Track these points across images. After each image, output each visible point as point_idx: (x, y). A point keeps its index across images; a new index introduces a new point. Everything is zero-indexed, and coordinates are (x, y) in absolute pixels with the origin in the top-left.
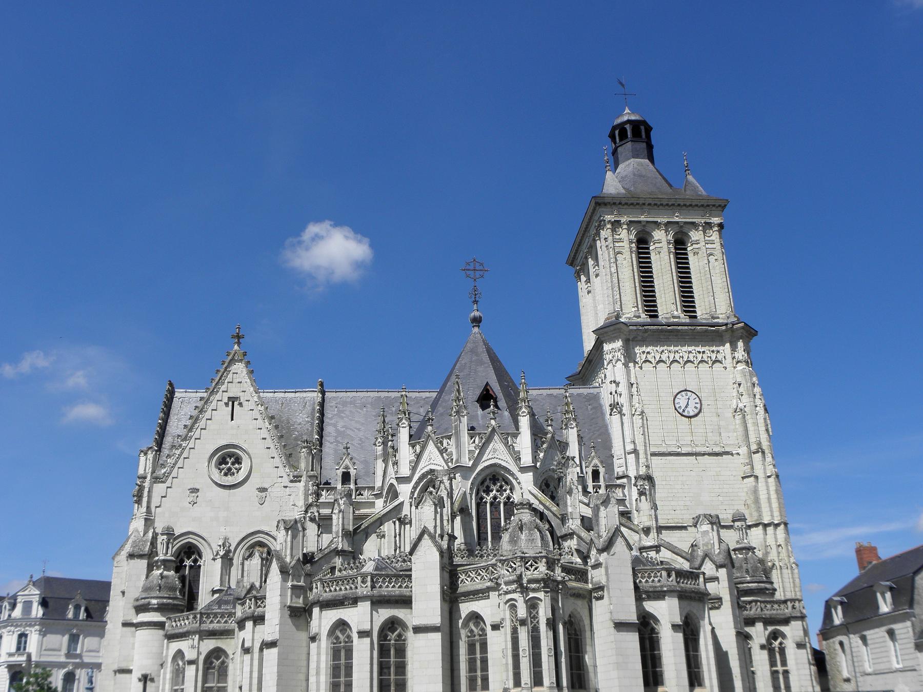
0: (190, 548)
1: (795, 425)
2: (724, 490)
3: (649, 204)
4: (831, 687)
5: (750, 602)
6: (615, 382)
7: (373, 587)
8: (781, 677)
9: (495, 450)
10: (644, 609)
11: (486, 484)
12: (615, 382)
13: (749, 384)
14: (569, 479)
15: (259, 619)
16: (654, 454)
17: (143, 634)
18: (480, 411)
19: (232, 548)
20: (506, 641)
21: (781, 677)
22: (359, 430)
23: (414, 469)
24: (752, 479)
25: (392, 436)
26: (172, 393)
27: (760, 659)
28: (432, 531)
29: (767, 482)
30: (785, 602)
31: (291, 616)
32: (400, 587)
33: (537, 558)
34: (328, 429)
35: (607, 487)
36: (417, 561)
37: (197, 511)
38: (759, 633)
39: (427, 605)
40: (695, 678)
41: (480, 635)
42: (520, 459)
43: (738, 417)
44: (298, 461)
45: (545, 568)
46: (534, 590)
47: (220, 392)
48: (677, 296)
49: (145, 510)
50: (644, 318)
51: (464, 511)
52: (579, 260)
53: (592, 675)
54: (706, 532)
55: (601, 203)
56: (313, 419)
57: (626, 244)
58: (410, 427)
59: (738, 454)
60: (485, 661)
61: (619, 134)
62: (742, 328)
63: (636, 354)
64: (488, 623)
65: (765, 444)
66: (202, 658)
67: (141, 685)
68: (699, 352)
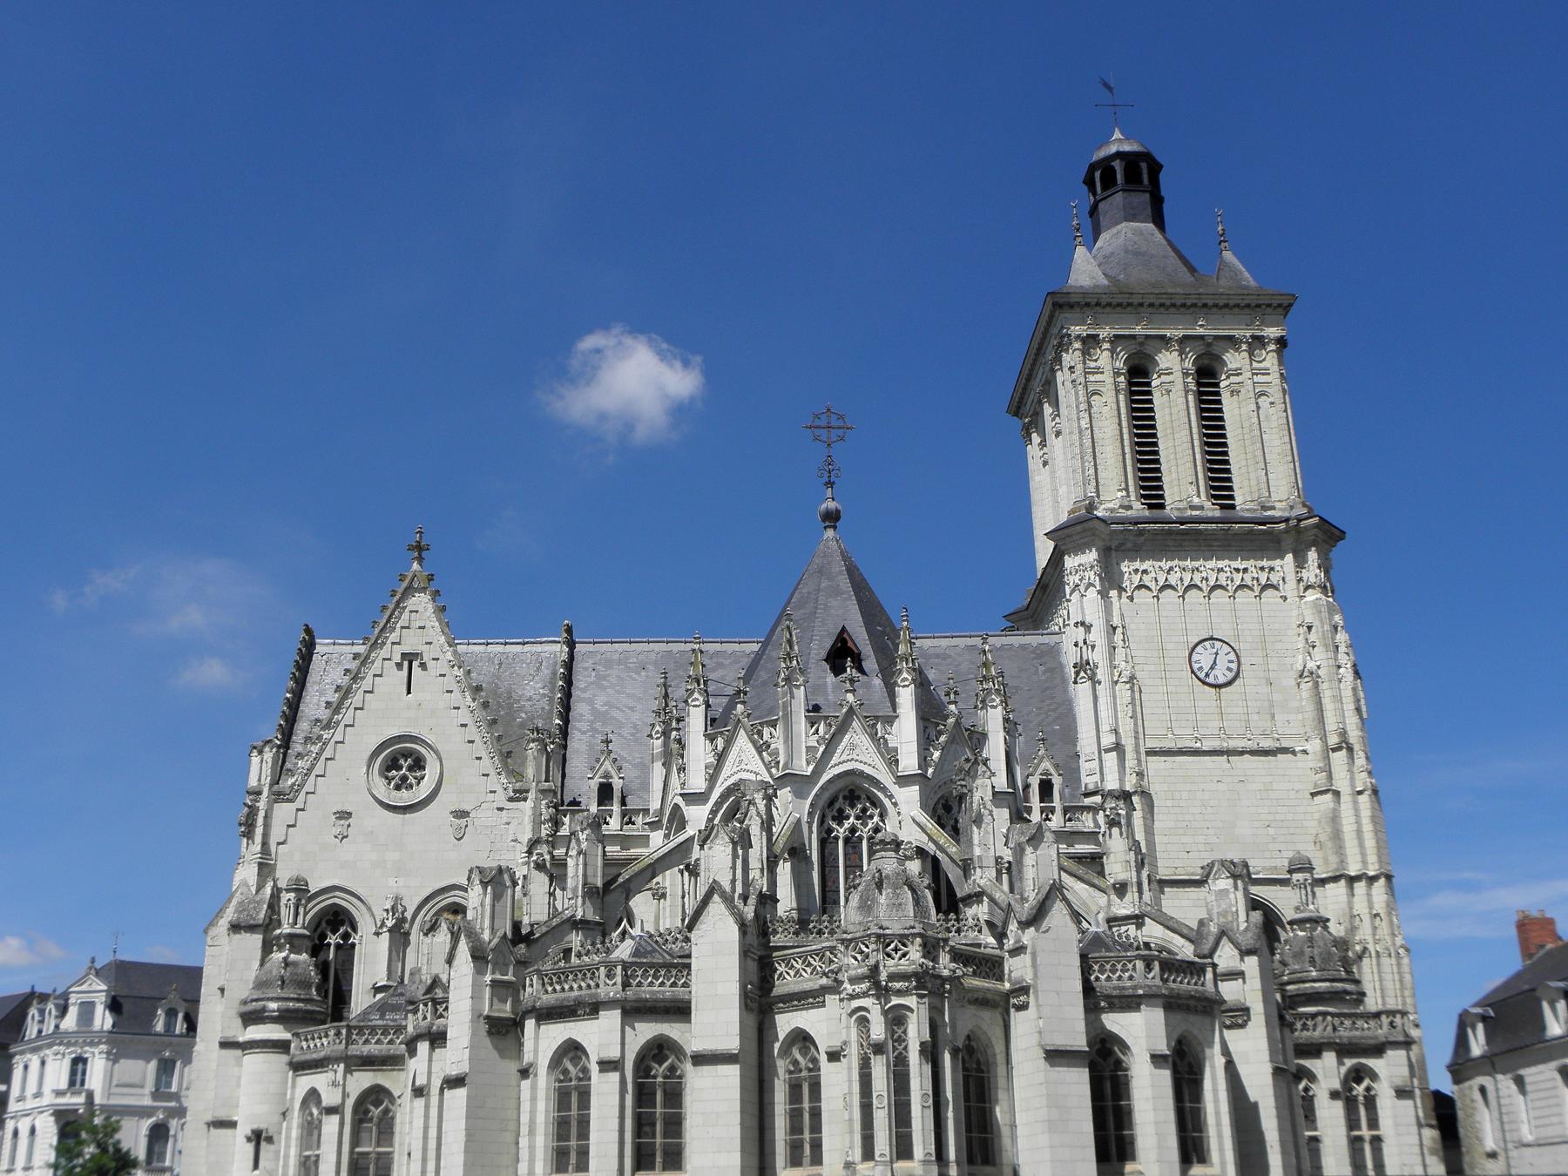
1: (1410, 704)
2: (1278, 817)
3: (1151, 305)
4: (1466, 1167)
5: (1314, 1016)
6: (1083, 624)
7: (626, 985)
9: (853, 747)
10: (1103, 1027)
11: (837, 806)
12: (1083, 624)
13: (1327, 627)
14: (976, 798)
15: (438, 1039)
16: (1151, 753)
17: (255, 1062)
18: (830, 678)
19: (408, 915)
20: (850, 1081)
22: (632, 709)
23: (712, 780)
24: (1329, 796)
25: (678, 720)
26: (308, 648)
27: (1330, 1119)
28: (728, 888)
29: (1355, 802)
30: (1377, 1015)
31: (490, 1033)
32: (674, 985)
33: (906, 936)
34: (579, 708)
35: (1066, 810)
37: (347, 850)
38: (1327, 1071)
39: (716, 1018)
40: (1191, 1147)
41: (810, 1070)
42: (897, 761)
43: (1306, 686)
44: (523, 764)
45: (919, 955)
46: (899, 993)
47: (389, 644)
48: (1199, 468)
49: (258, 848)
50: (1138, 509)
51: (796, 852)
52: (1028, 407)
53: (1006, 1141)
54: (1224, 892)
55: (1063, 303)
56: (552, 691)
57: (1107, 377)
58: (708, 706)
59: (1305, 752)
60: (816, 1114)
61: (1102, 177)
62: (1316, 526)
63: (1122, 574)
64: (822, 1049)
65: (1354, 735)
66: (350, 1103)
67: (250, 1147)
68: (1237, 570)
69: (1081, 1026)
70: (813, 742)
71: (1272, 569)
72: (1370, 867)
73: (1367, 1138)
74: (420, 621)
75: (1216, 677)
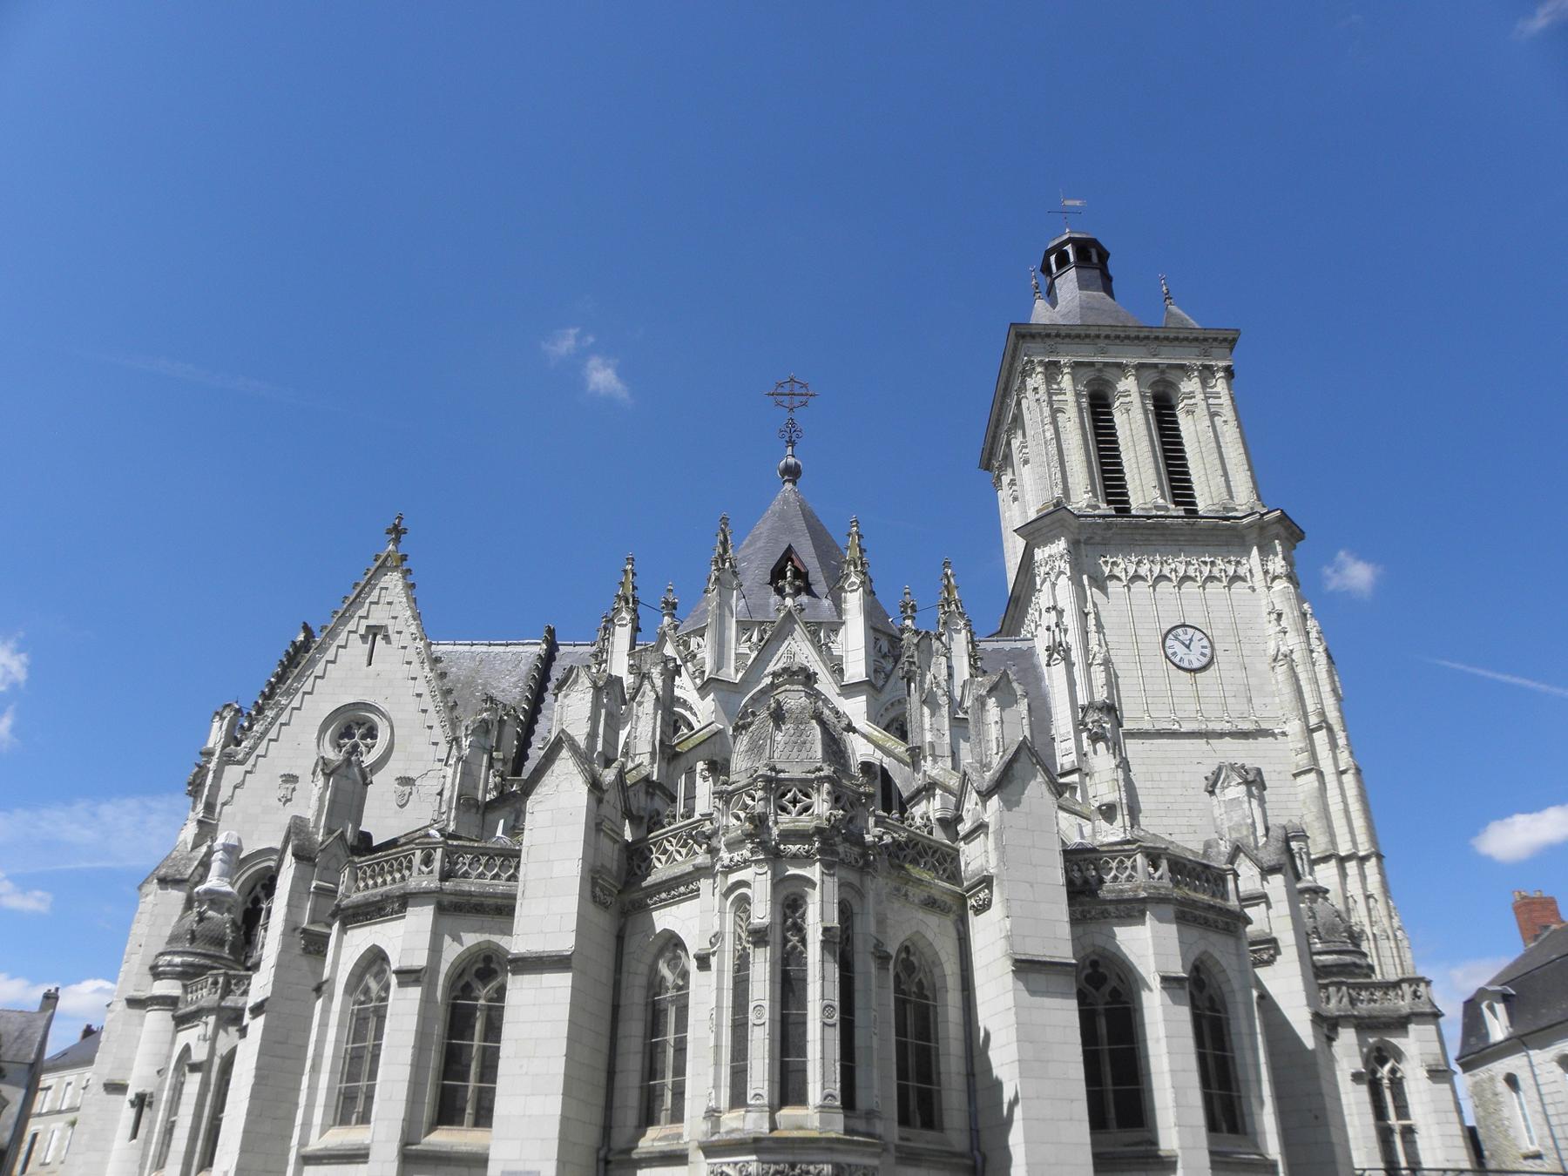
0: (488, 959)
3: (1107, 337)
7: (445, 876)
8: (1398, 1139)
17: (157, 1019)
21: (1398, 1139)
24: (1312, 776)
27: (1354, 1103)
28: (582, 742)
29: (1341, 784)
30: (1396, 985)
36: (538, 808)
40: (1225, 1109)
46: (795, 859)
55: (1024, 334)
57: (1070, 397)
59: (1284, 734)
64: (692, 951)
65: (1333, 716)
69: (1064, 929)
70: (744, 649)
71: (1238, 563)
72: (1360, 847)
73: (1397, 1129)
74: (390, 601)
75: (1190, 662)
